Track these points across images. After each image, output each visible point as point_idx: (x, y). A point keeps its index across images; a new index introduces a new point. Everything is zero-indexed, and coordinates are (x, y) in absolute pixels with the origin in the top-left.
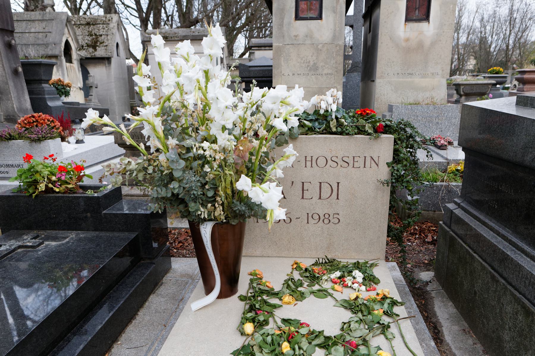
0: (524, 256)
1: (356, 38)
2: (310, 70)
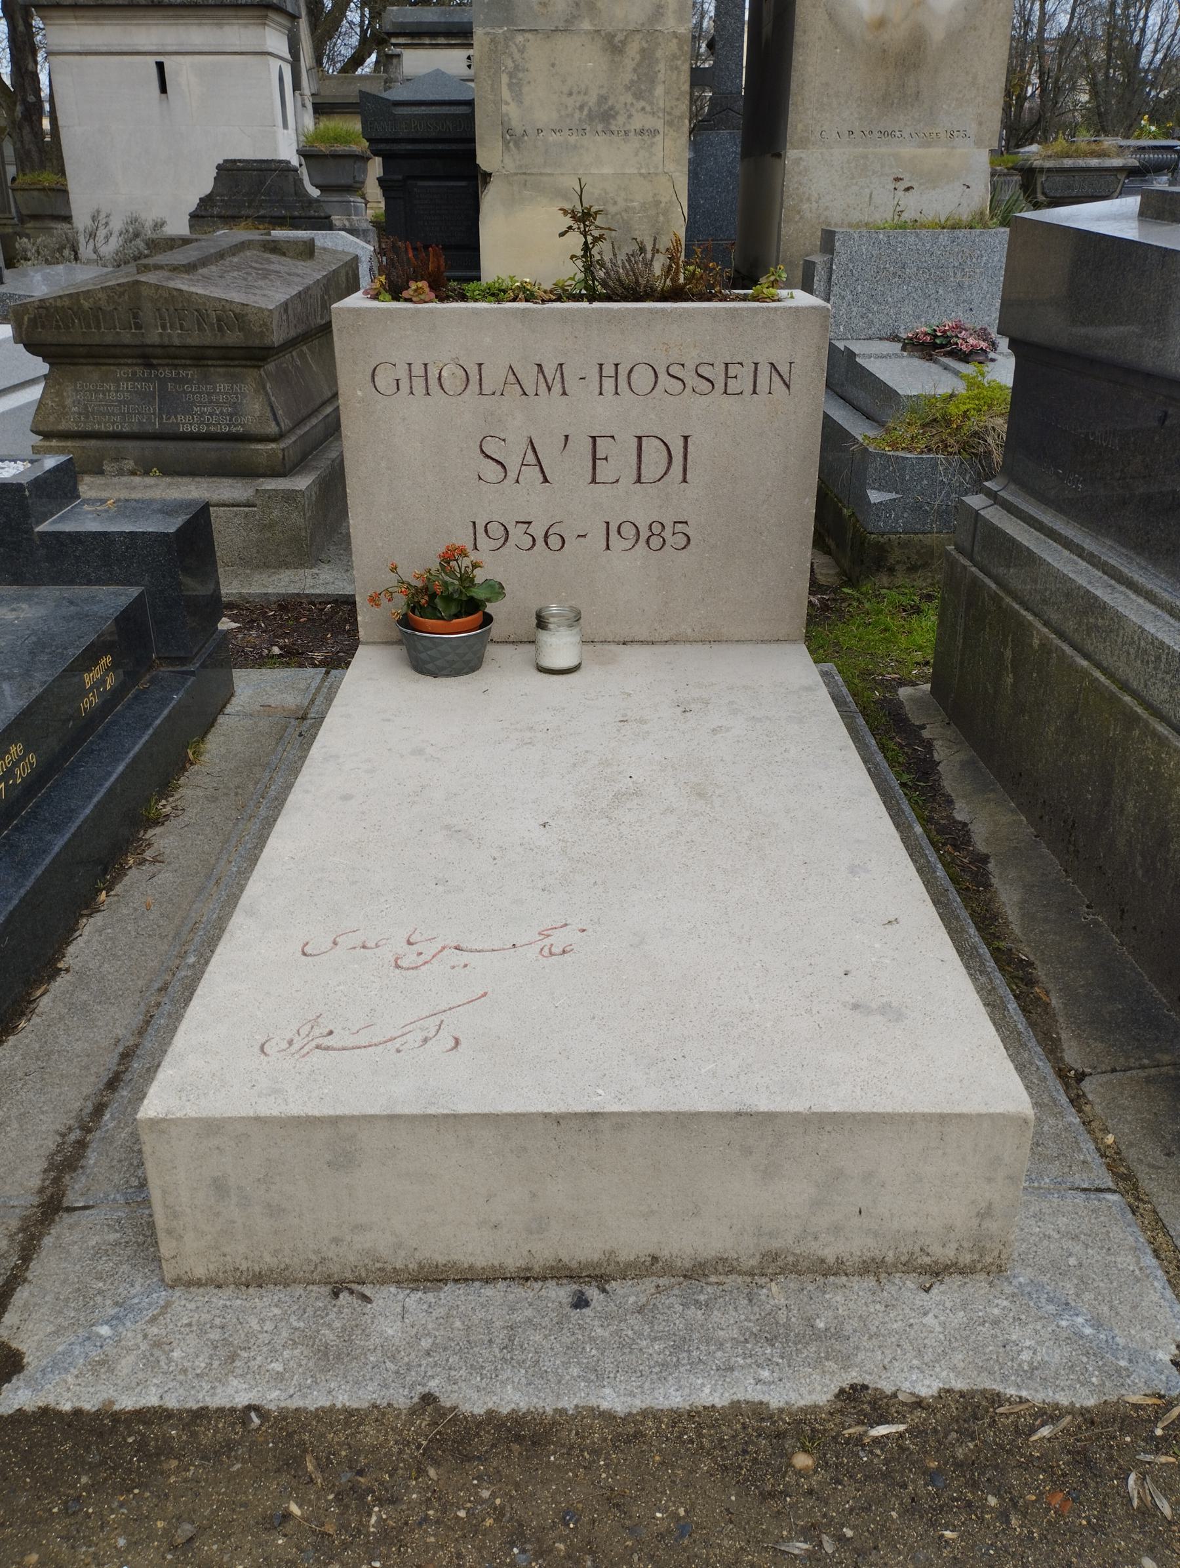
0: (1133, 596)
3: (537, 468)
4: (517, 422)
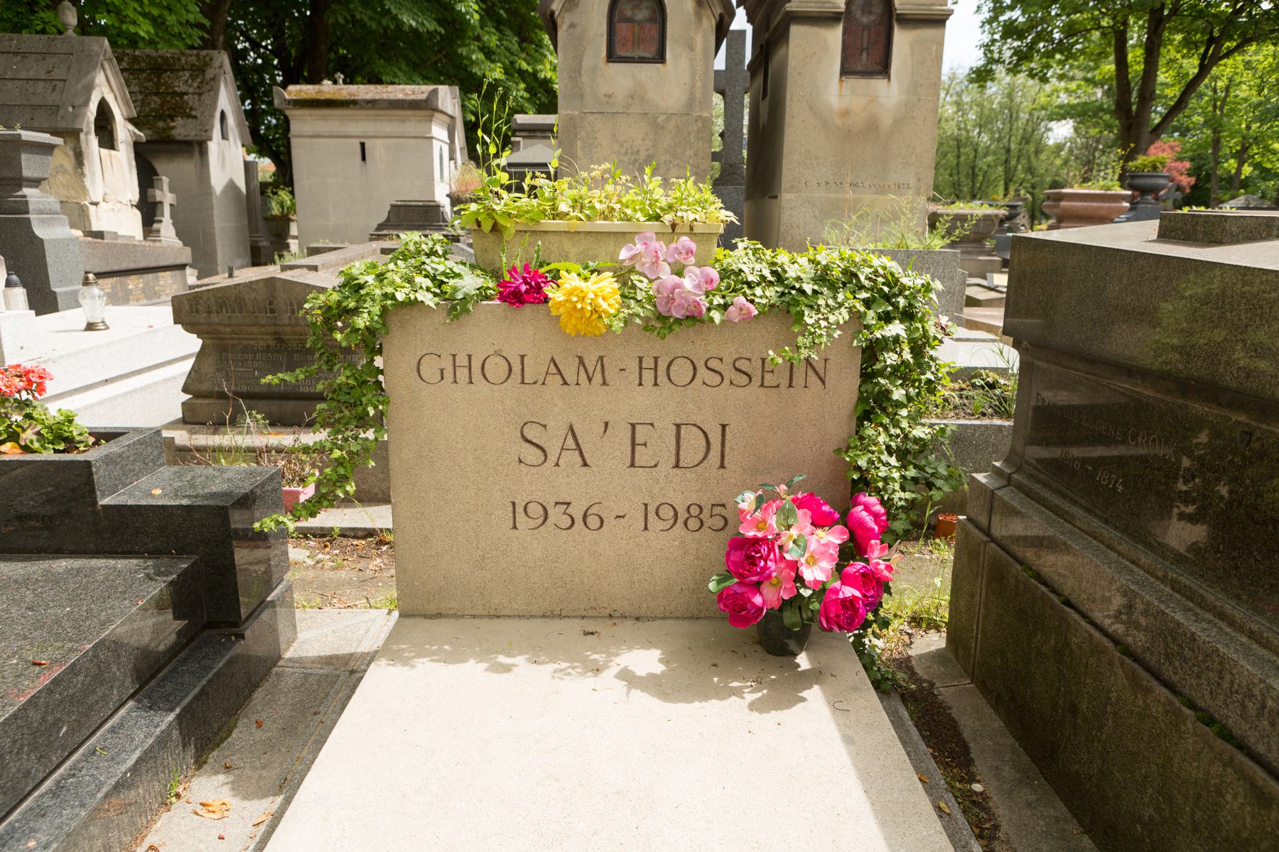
1: (732, 115)
3: (577, 453)
4: (558, 407)
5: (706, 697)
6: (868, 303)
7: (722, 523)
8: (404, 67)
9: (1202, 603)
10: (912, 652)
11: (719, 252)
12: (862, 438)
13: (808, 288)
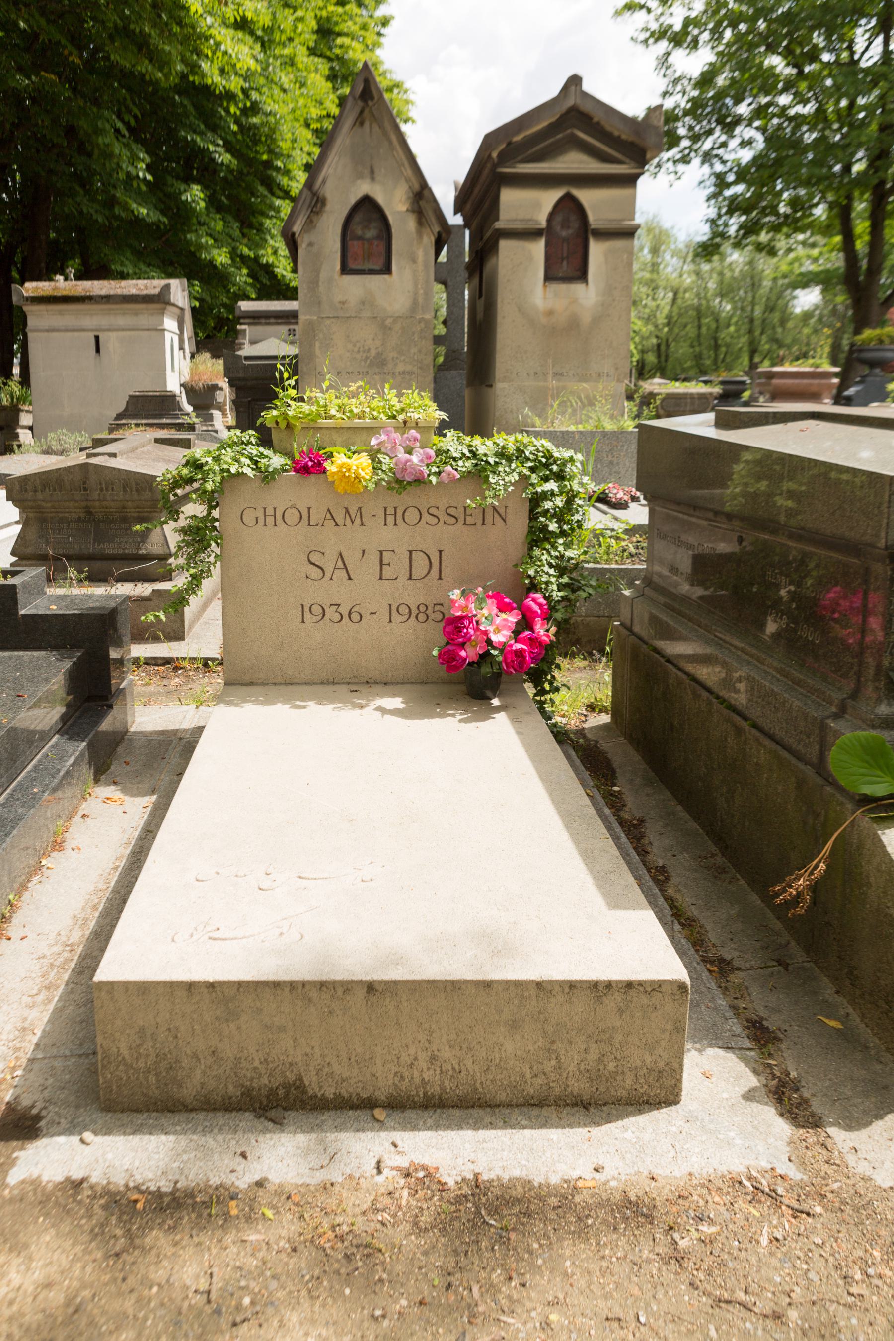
1: (454, 301)
2: (371, 365)
4: (331, 541)
5: (432, 717)
6: (533, 470)
7: (441, 617)
8: (128, 254)
9: (680, 613)
10: (586, 725)
11: (436, 439)
12: (531, 557)
13: (492, 460)
